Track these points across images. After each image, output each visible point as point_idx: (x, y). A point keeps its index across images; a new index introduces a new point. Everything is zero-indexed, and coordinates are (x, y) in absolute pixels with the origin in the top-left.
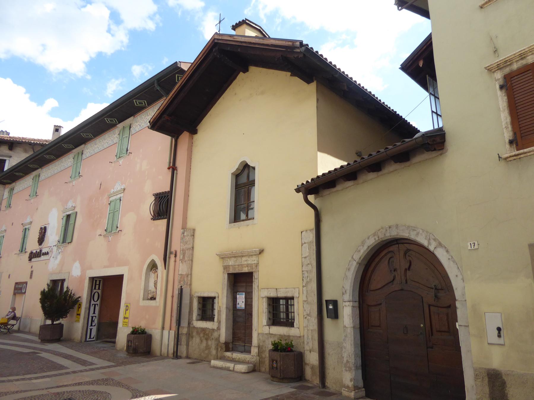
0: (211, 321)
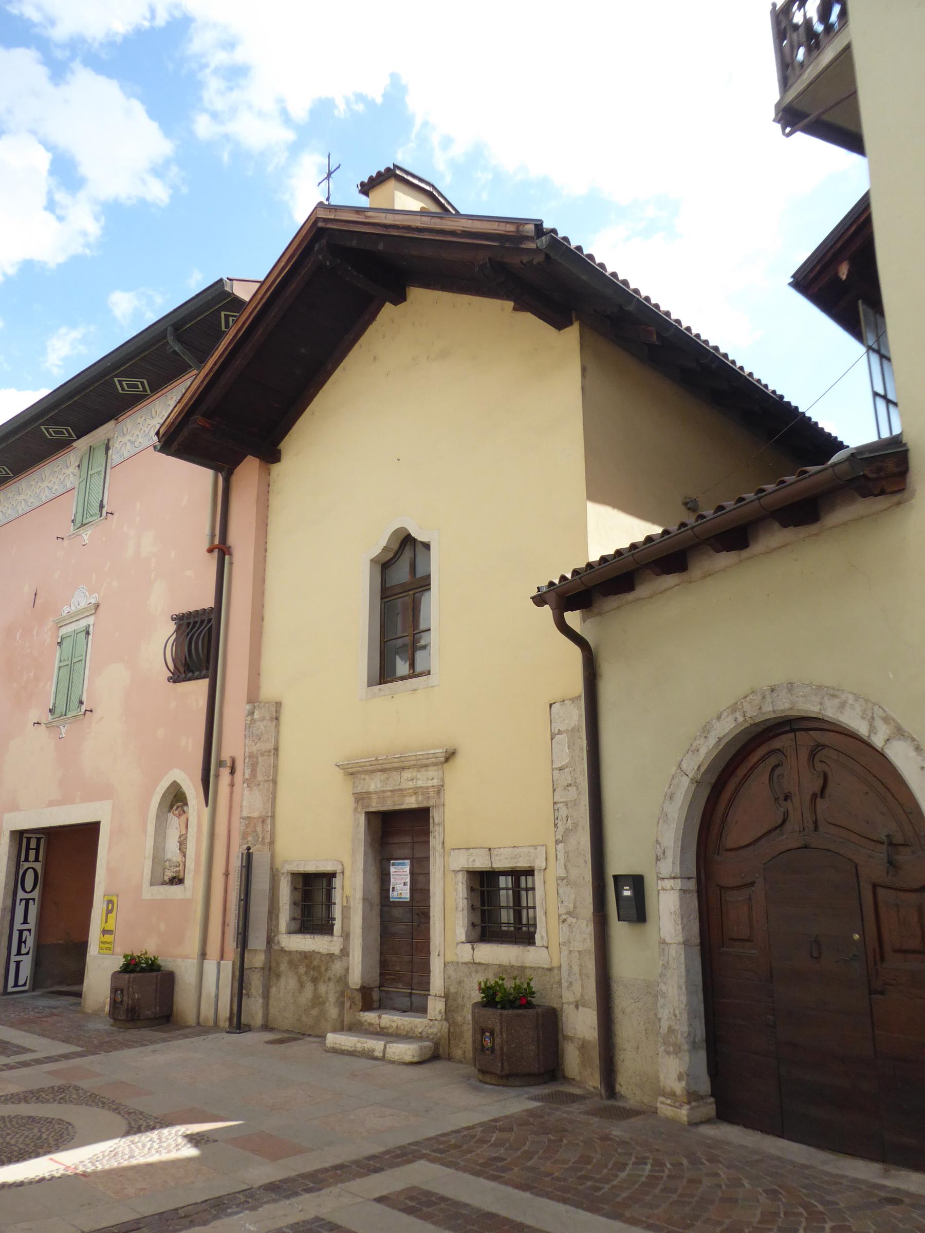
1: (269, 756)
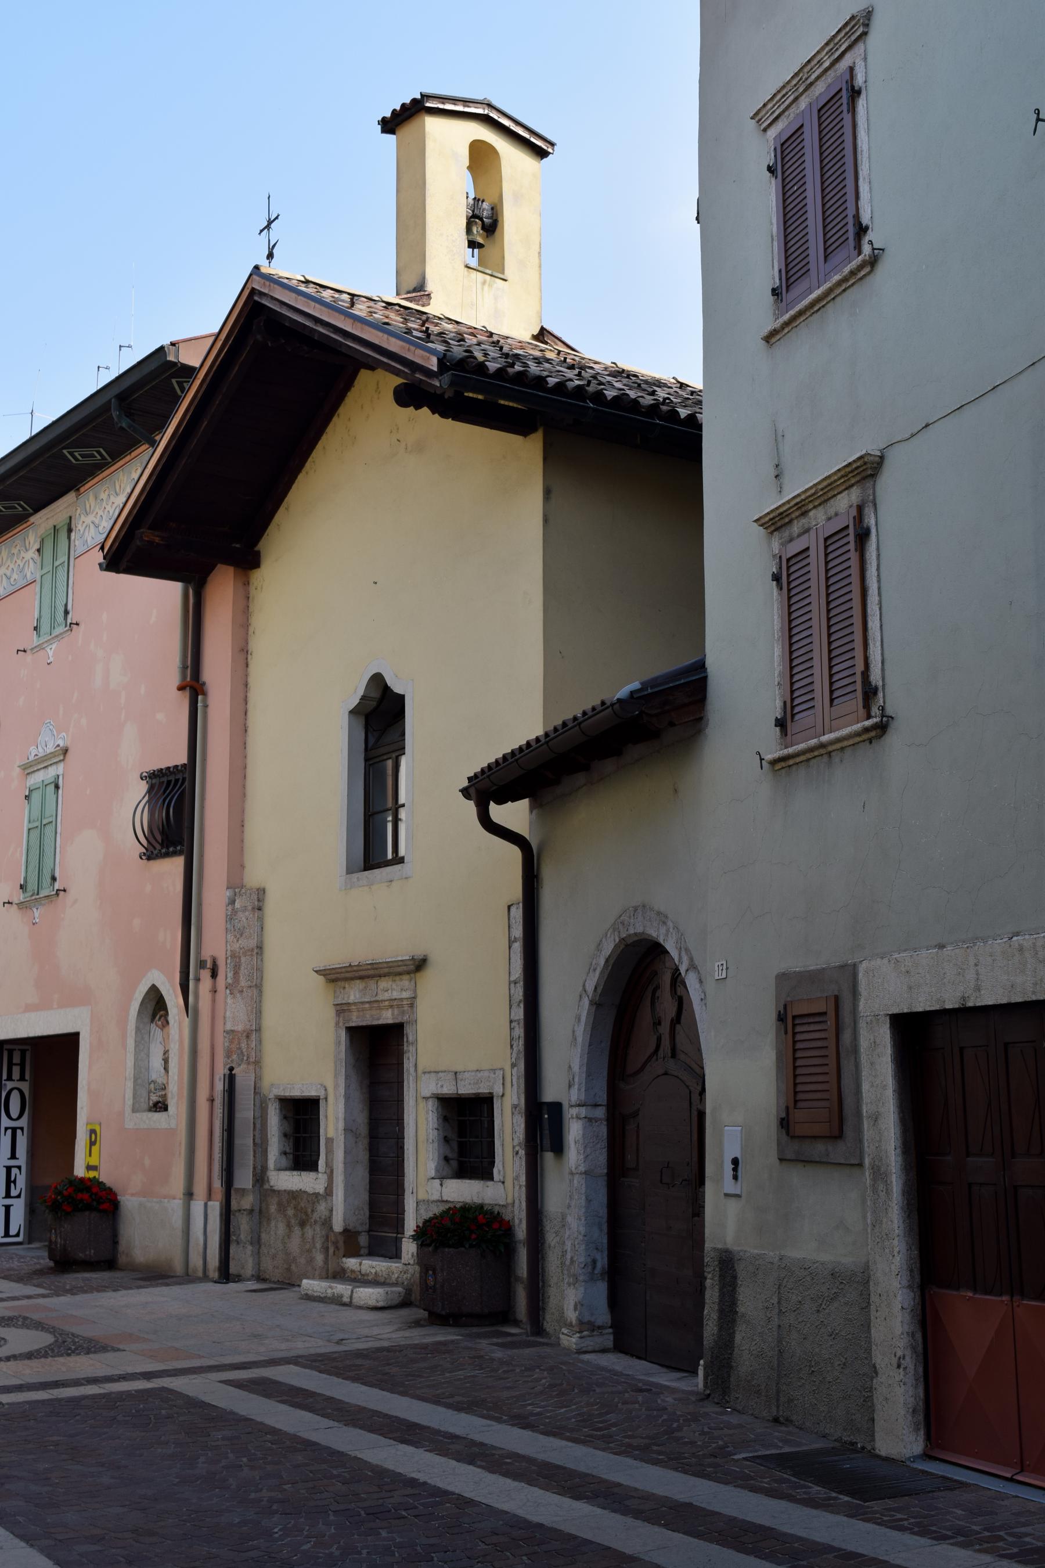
0: (311, 1171)
1: (252, 955)
